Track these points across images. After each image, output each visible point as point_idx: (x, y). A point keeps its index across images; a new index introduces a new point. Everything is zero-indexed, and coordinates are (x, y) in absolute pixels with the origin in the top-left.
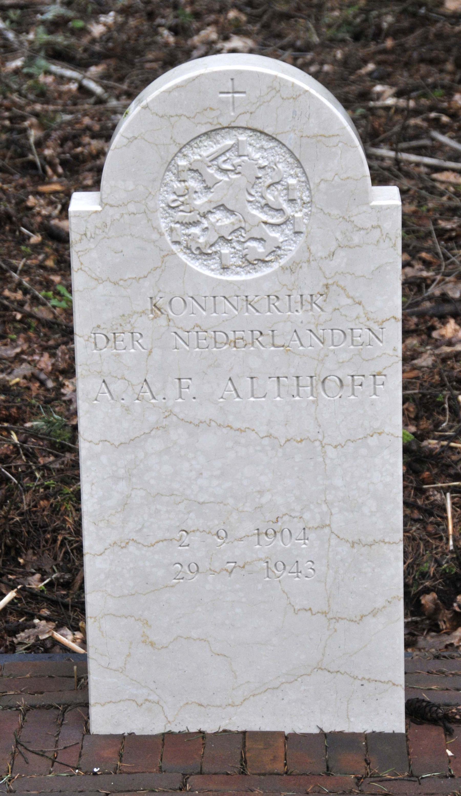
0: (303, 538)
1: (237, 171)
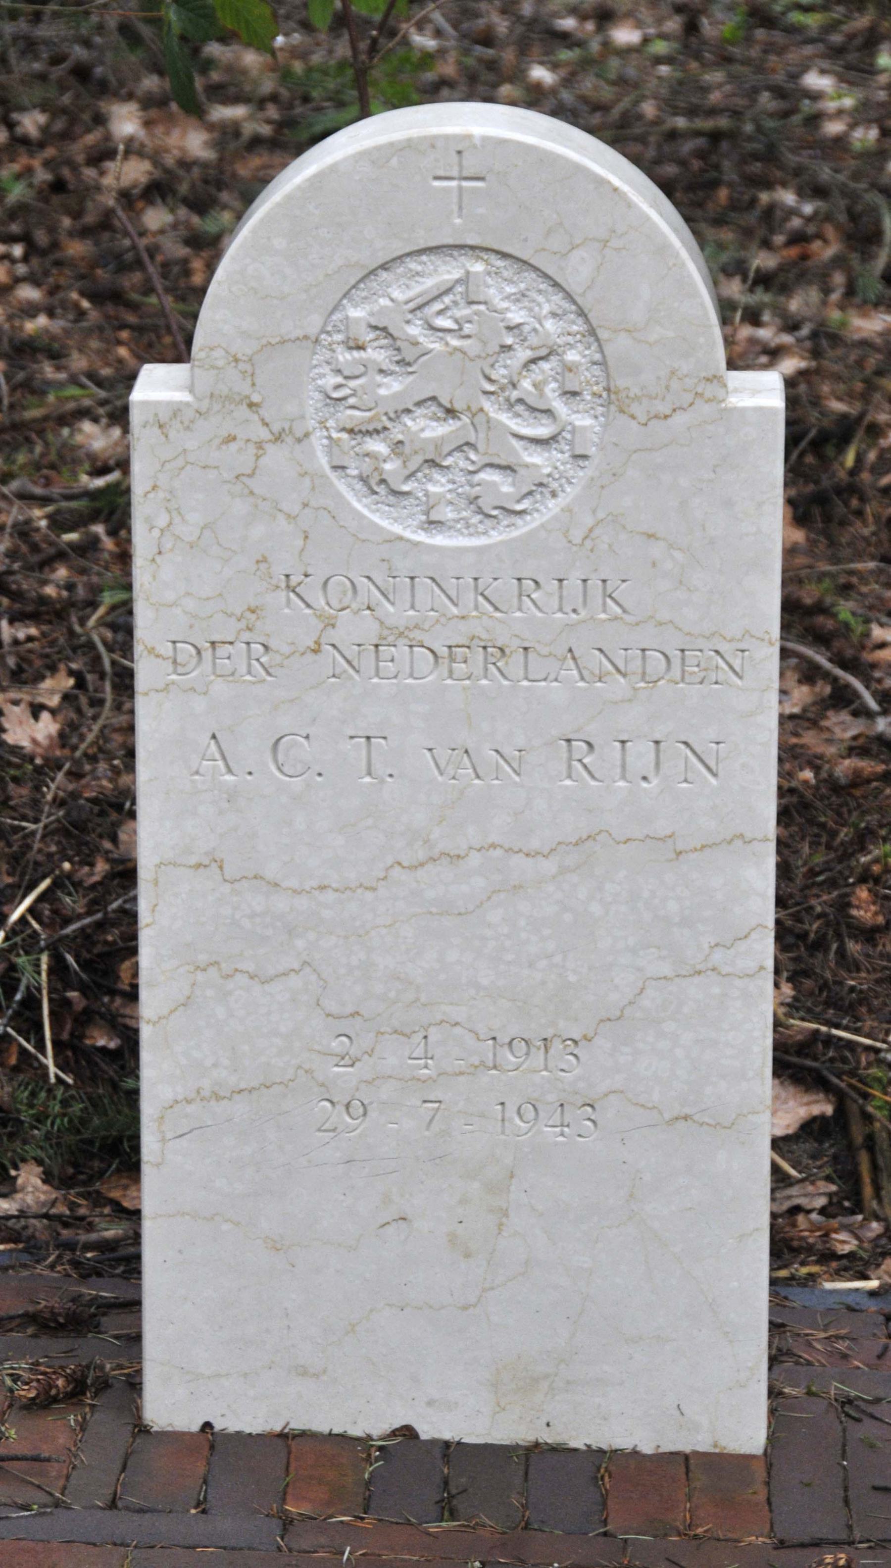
1: (463, 333)
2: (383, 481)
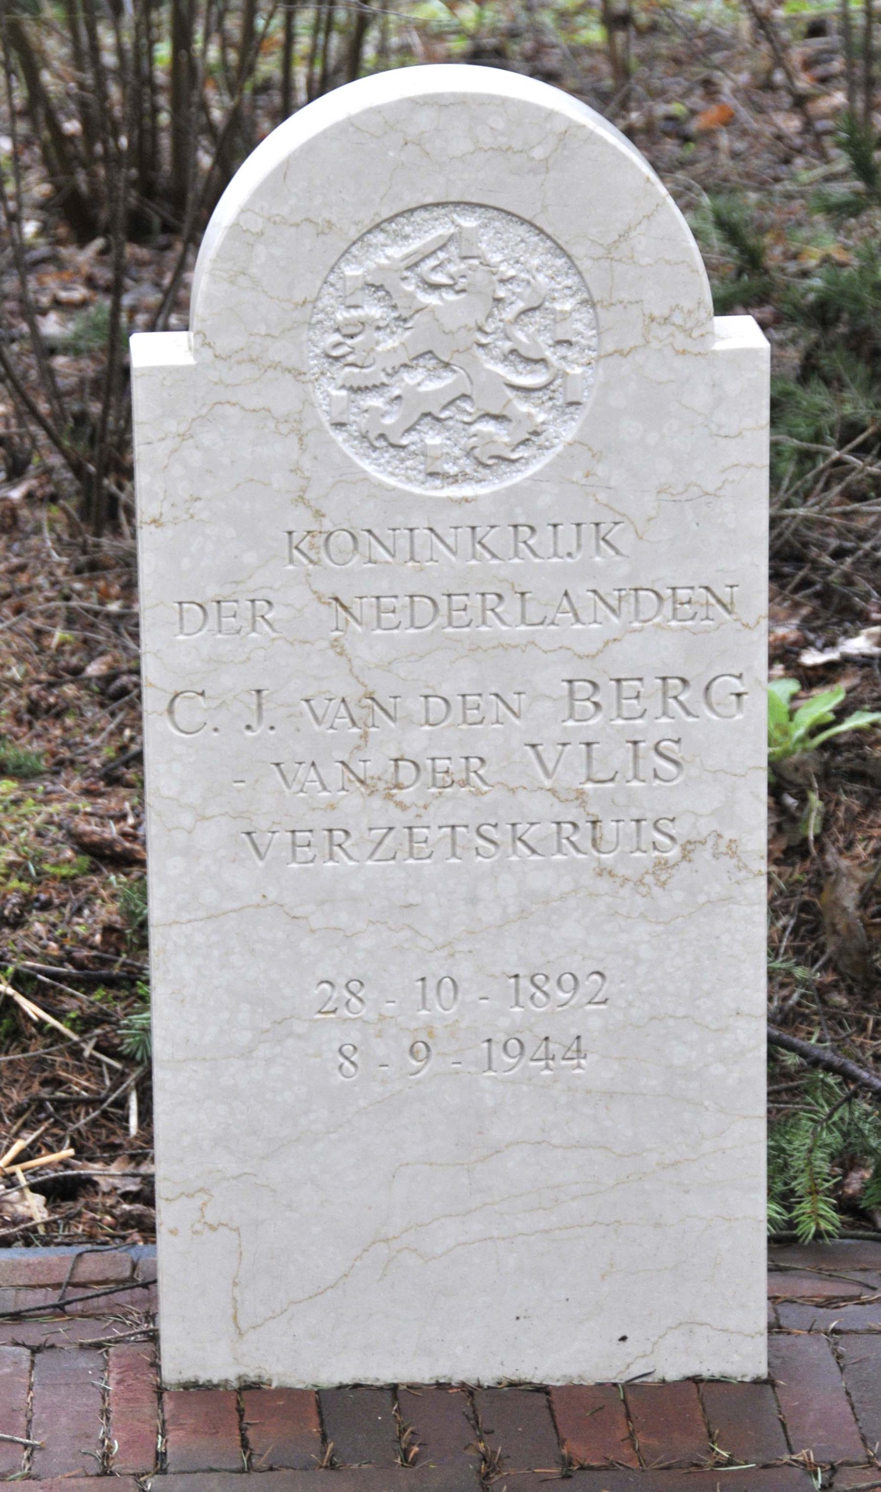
0: (543, 1057)
1: (457, 288)
2: (382, 436)
